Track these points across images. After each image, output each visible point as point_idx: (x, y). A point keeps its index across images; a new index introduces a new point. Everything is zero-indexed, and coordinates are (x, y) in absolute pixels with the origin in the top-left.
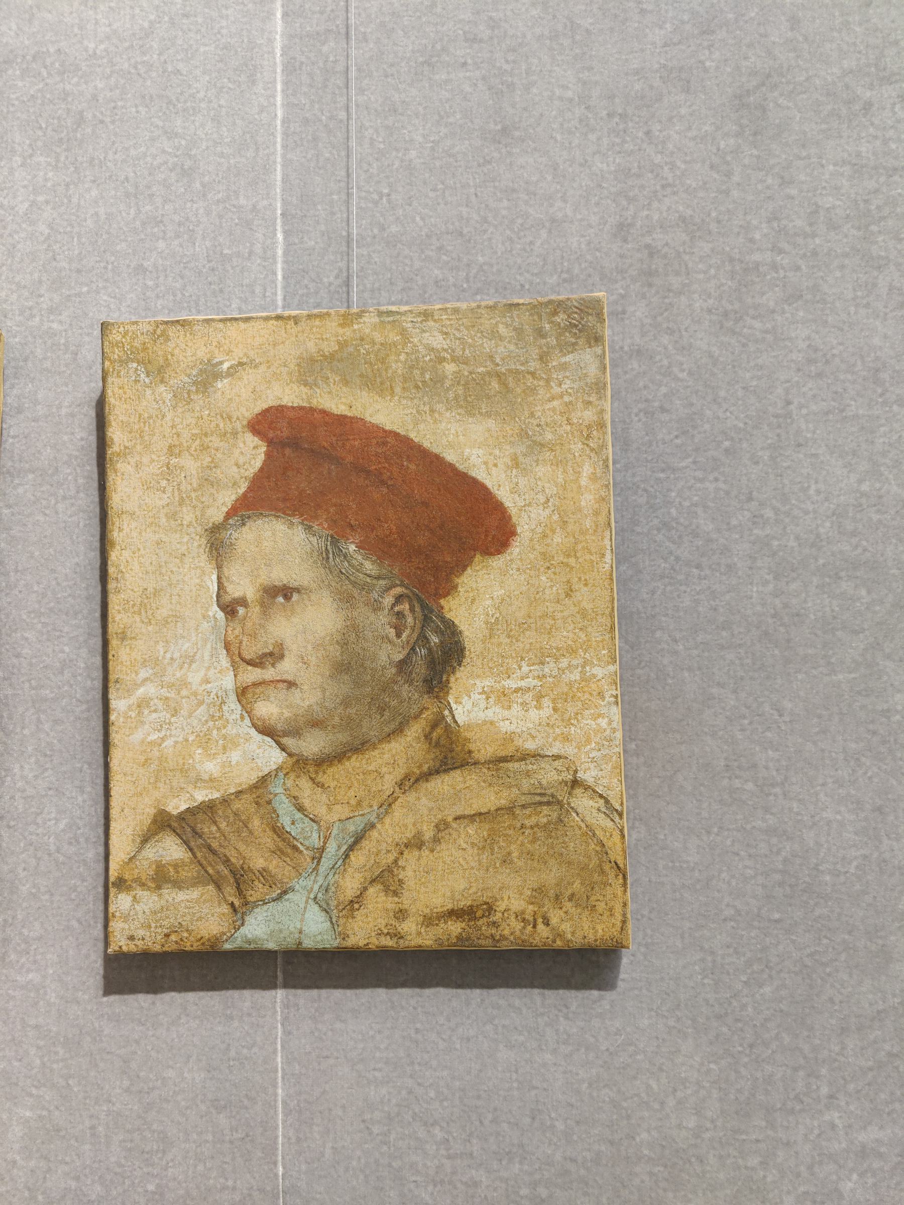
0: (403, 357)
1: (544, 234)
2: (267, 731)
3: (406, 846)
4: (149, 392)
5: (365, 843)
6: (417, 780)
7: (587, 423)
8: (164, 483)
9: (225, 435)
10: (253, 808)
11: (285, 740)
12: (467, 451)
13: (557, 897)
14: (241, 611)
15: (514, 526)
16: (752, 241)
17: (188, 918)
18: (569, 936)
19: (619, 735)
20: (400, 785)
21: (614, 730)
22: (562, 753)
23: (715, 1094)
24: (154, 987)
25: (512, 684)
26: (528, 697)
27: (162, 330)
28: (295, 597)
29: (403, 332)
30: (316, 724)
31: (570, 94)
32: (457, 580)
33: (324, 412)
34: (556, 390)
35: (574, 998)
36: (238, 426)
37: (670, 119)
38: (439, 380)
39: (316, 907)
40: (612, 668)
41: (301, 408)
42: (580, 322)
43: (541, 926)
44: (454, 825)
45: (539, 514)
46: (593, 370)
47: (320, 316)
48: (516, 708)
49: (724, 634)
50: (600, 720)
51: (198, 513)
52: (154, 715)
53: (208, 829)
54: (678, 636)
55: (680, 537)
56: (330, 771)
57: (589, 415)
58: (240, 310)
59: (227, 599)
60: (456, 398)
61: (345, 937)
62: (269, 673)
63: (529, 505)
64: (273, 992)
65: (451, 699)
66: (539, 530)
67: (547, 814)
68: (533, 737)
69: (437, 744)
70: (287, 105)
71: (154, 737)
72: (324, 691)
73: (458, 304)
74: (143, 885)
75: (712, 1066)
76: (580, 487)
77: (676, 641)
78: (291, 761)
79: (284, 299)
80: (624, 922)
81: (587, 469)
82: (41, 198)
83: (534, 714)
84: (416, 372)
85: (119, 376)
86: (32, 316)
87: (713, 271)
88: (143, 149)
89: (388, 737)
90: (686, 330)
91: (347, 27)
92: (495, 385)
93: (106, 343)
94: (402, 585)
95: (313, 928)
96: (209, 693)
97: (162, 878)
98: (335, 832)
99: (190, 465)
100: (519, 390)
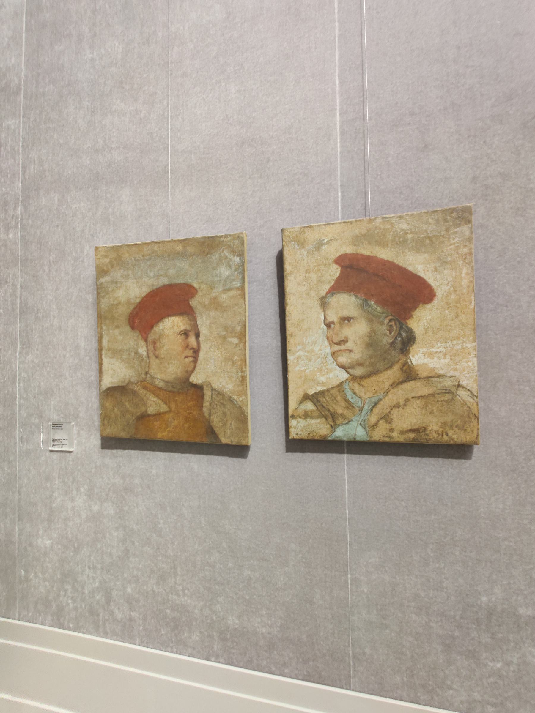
0: (391, 233)
1: (442, 184)
2: (342, 367)
3: (394, 407)
4: (298, 252)
5: (378, 406)
6: (398, 384)
7: (464, 253)
8: (304, 283)
9: (326, 265)
10: (338, 393)
11: (349, 370)
12: (416, 266)
13: (451, 426)
14: (332, 326)
15: (435, 293)
16: (529, 180)
17: (316, 429)
18: (456, 440)
19: (476, 368)
20: (391, 386)
21: (475, 367)
22: (454, 375)
23: (510, 497)
24: (303, 451)
25: (434, 350)
26: (440, 355)
27: (302, 230)
28: (352, 321)
29: (392, 224)
30: (360, 364)
31: (452, 130)
32: (413, 313)
33: (362, 255)
34: (453, 242)
35: (455, 462)
36: (330, 261)
37: (494, 135)
38: (405, 241)
39: (361, 427)
40: (474, 344)
41: (353, 254)
42: (463, 215)
43: (445, 436)
44: (412, 400)
45: (445, 288)
46: (467, 233)
47: (360, 221)
48: (436, 359)
49: (517, 331)
50: (469, 363)
51: (317, 293)
52: (303, 362)
53: (322, 399)
54: (497, 332)
55: (499, 295)
56: (365, 381)
57: (466, 250)
58: (326, 221)
59: (327, 322)
60: (412, 247)
61: (371, 437)
62: (343, 347)
63: (441, 285)
64: (342, 455)
65: (410, 356)
66: (445, 294)
67: (447, 397)
68: (442, 369)
69: (405, 372)
70: (342, 147)
71: (303, 369)
72: (363, 353)
73: (413, 212)
74: (300, 417)
75: (509, 487)
76: (462, 278)
77: (496, 334)
78: (351, 377)
79: (342, 216)
80: (478, 436)
81: (464, 271)
82: (256, 189)
83: (443, 361)
84: (397, 239)
85: (288, 247)
86: (254, 229)
87: (513, 193)
88: (290, 168)
89: (387, 369)
90: (502, 216)
91: (364, 115)
92: (428, 241)
93: (284, 236)
94: (391, 315)
95: (359, 433)
96: (321, 354)
97: (306, 415)
98: (367, 401)
99: (314, 276)
100: (437, 243)
